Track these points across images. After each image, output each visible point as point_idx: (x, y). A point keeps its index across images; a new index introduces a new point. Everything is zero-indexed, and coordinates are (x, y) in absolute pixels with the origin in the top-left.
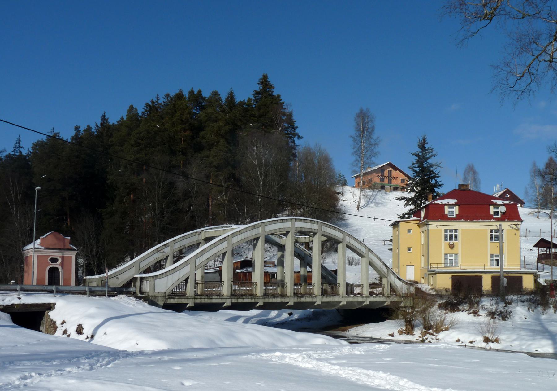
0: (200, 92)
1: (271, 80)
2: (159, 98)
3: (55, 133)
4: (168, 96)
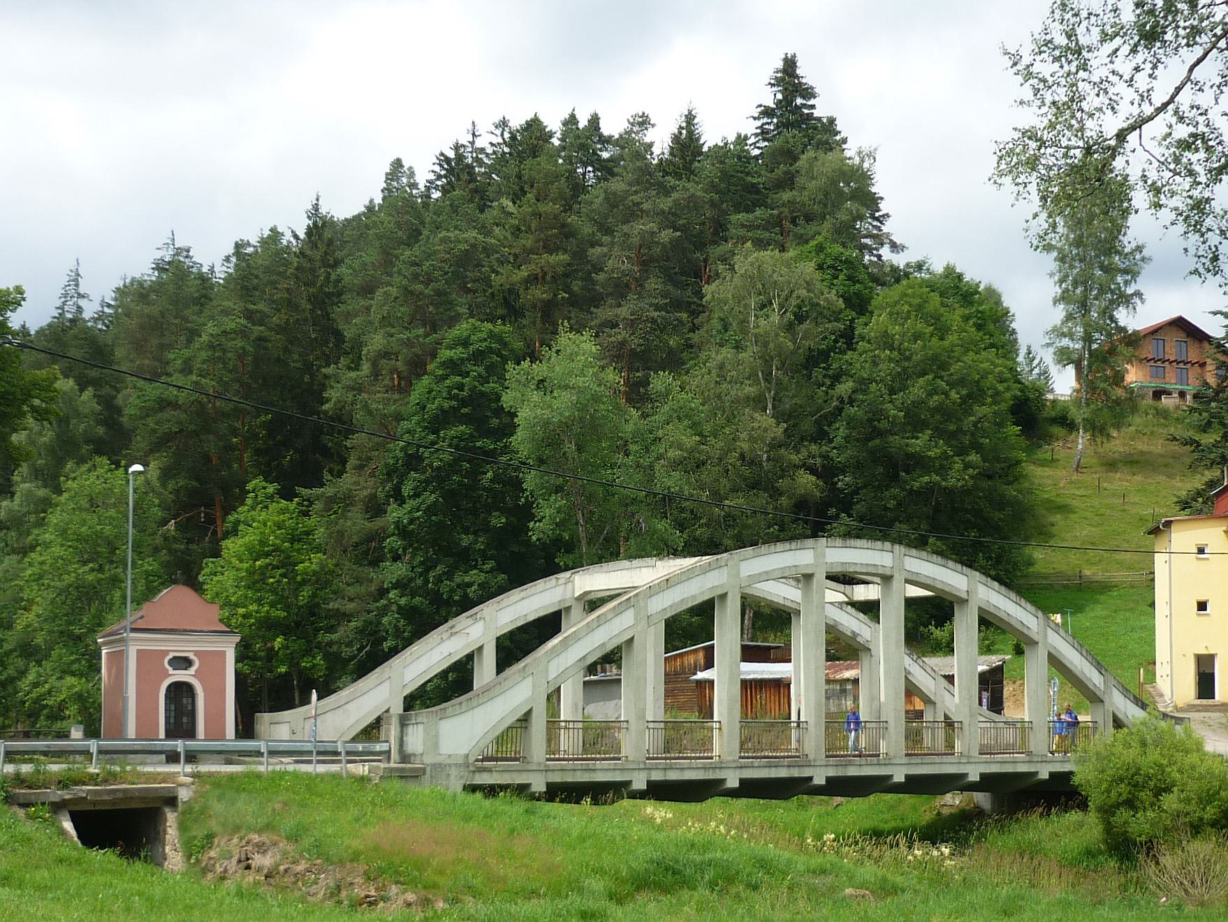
0: (595, 121)
1: (807, 73)
2: (477, 133)
3: (177, 249)
4: (503, 124)
